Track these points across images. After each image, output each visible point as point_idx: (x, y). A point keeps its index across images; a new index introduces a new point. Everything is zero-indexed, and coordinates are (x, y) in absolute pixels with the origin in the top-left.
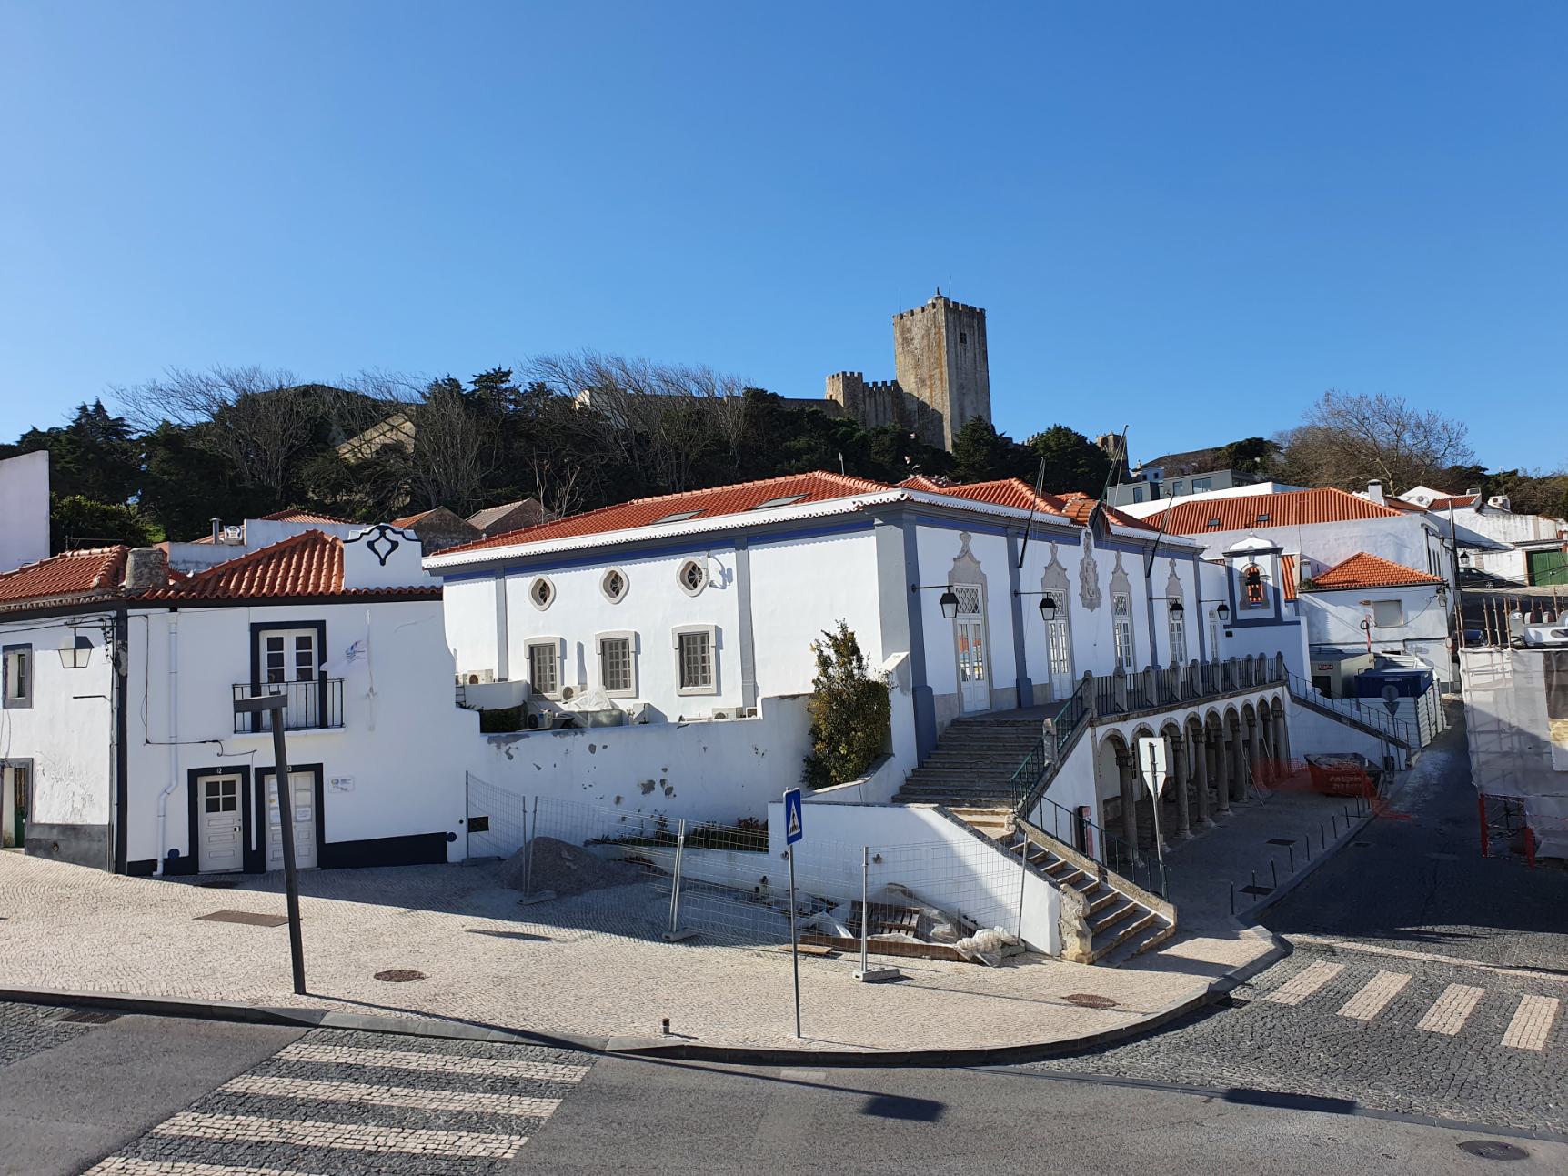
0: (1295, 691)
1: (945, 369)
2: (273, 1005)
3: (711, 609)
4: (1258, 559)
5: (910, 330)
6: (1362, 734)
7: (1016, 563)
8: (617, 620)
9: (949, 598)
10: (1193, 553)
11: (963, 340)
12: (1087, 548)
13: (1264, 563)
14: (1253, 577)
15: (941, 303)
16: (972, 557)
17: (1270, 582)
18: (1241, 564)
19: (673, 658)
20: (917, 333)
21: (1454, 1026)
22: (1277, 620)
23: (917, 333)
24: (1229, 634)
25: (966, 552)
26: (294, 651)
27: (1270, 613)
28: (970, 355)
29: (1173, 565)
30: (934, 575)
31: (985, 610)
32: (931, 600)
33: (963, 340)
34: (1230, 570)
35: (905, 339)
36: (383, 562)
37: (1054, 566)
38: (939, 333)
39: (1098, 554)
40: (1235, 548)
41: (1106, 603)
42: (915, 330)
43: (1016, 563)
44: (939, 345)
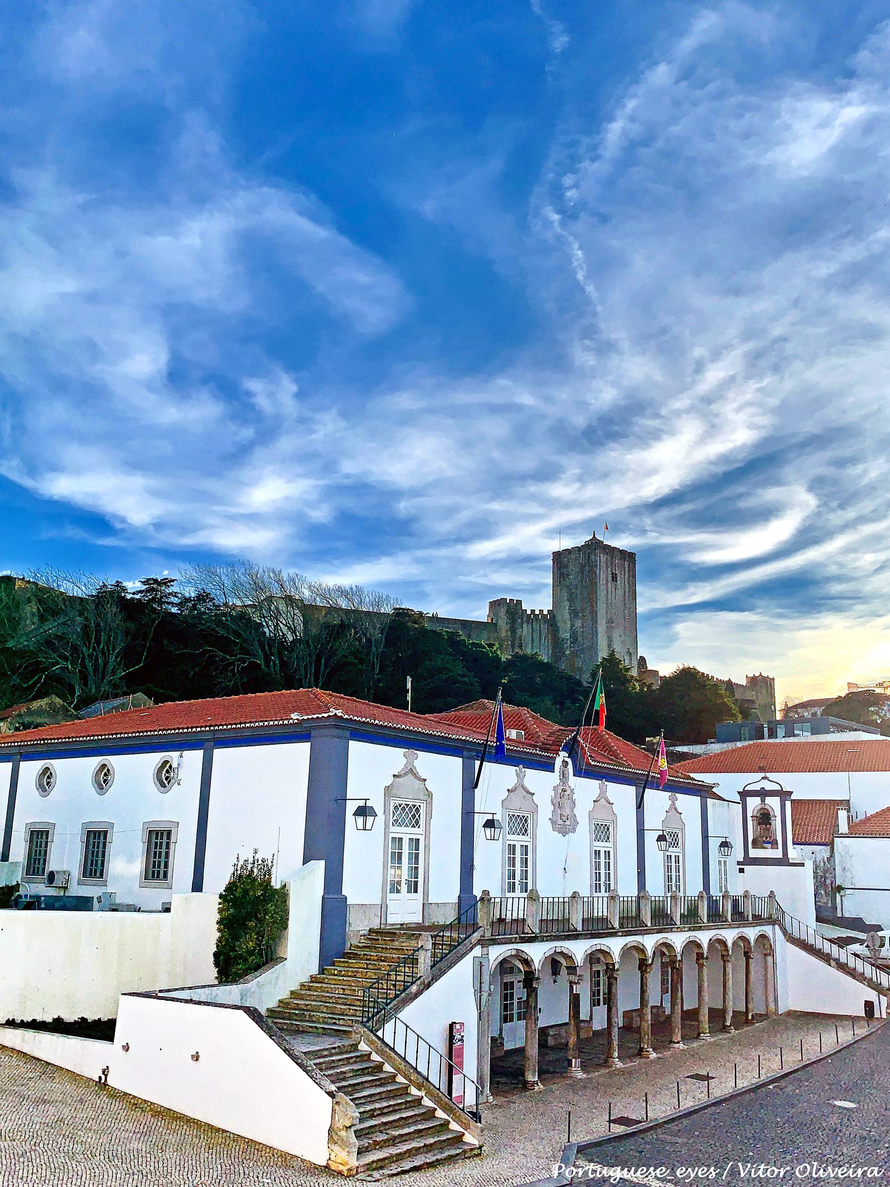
3: (178, 807)
4: (768, 800)
5: (566, 566)
6: (803, 954)
7: (471, 784)
8: (98, 810)
9: (661, 838)
10: (705, 792)
11: (614, 578)
12: (564, 776)
13: (773, 803)
16: (676, 809)
19: (140, 848)
22: (784, 861)
24: (742, 871)
25: (603, 794)
26: (408, 851)
27: (778, 854)
28: (620, 593)
29: (673, 800)
30: (654, 820)
31: (683, 845)
32: (650, 838)
33: (614, 578)
37: (520, 789)
39: (575, 782)
41: (584, 829)
42: (571, 567)
43: (471, 784)
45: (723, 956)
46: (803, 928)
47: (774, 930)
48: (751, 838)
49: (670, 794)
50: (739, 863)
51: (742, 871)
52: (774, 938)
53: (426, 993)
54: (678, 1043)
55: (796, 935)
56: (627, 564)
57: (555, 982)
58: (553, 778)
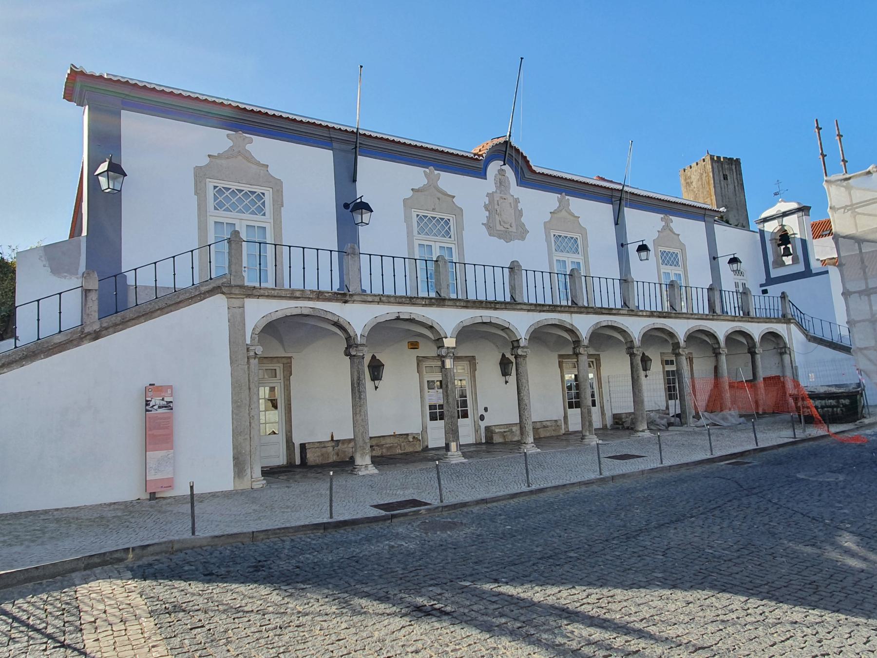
0: (811, 333)
1: (714, 197)
2: (618, 441)
4: (786, 221)
5: (690, 178)
11: (725, 177)
12: (501, 183)
14: (784, 238)
15: (708, 159)
16: (671, 230)
17: (798, 236)
18: (771, 227)
20: (695, 178)
21: (261, 389)
23: (695, 178)
27: (800, 268)
28: (731, 187)
33: (725, 177)
34: (762, 233)
35: (687, 183)
36: (98, 94)
38: (708, 175)
40: (764, 215)
42: (693, 177)
44: (709, 183)
45: (714, 349)
46: (826, 326)
47: (789, 330)
48: (771, 259)
49: (662, 216)
50: (761, 286)
51: (765, 292)
52: (790, 339)
53: (87, 348)
54: (643, 431)
55: (819, 334)
56: (734, 167)
57: (506, 382)
58: (488, 185)
